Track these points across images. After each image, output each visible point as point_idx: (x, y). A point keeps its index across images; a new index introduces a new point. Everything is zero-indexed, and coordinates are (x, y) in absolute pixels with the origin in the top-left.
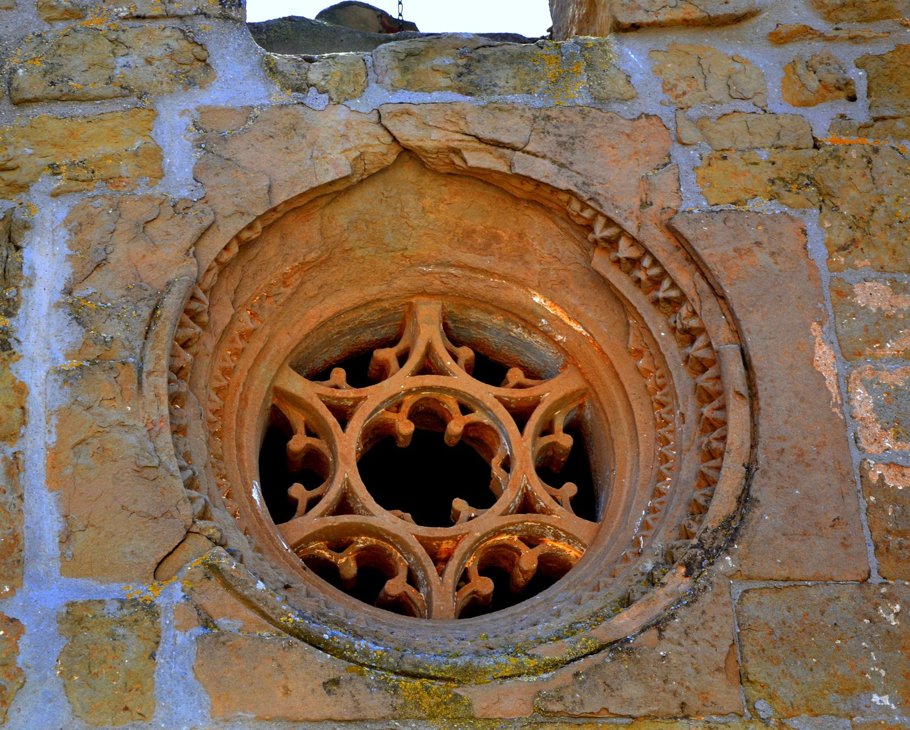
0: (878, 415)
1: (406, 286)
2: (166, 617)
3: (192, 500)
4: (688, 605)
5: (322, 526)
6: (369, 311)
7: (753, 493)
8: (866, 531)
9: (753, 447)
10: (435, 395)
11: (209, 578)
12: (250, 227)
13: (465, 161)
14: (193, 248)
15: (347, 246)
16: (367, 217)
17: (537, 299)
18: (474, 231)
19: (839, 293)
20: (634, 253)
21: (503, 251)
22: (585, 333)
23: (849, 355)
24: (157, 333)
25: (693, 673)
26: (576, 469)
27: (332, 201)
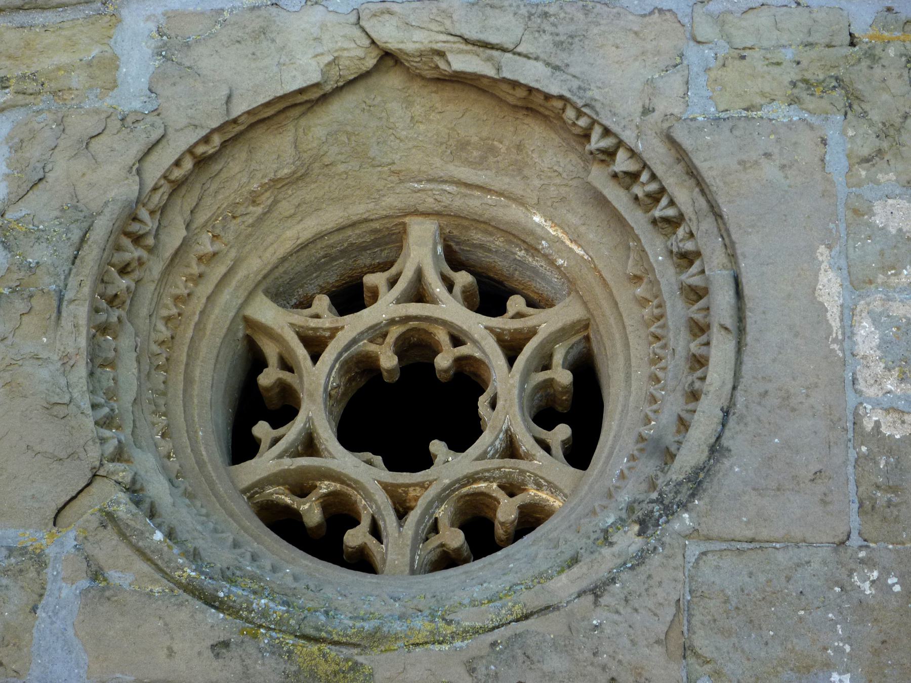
0: (882, 352)
1: (395, 204)
2: (54, 568)
3: (103, 441)
4: (632, 568)
5: (277, 469)
6: (357, 232)
7: (725, 442)
8: (852, 487)
9: (734, 388)
10: (424, 325)
11: (105, 527)
12: (206, 140)
13: (449, 64)
14: (137, 165)
15: (326, 160)
16: (349, 128)
17: (537, 219)
18: (468, 143)
19: (856, 212)
20: (632, 167)
21: (501, 165)
22: (586, 257)
23: (857, 283)
24: (83, 258)
25: (628, 644)
26: (576, 412)
27: (309, 109)
